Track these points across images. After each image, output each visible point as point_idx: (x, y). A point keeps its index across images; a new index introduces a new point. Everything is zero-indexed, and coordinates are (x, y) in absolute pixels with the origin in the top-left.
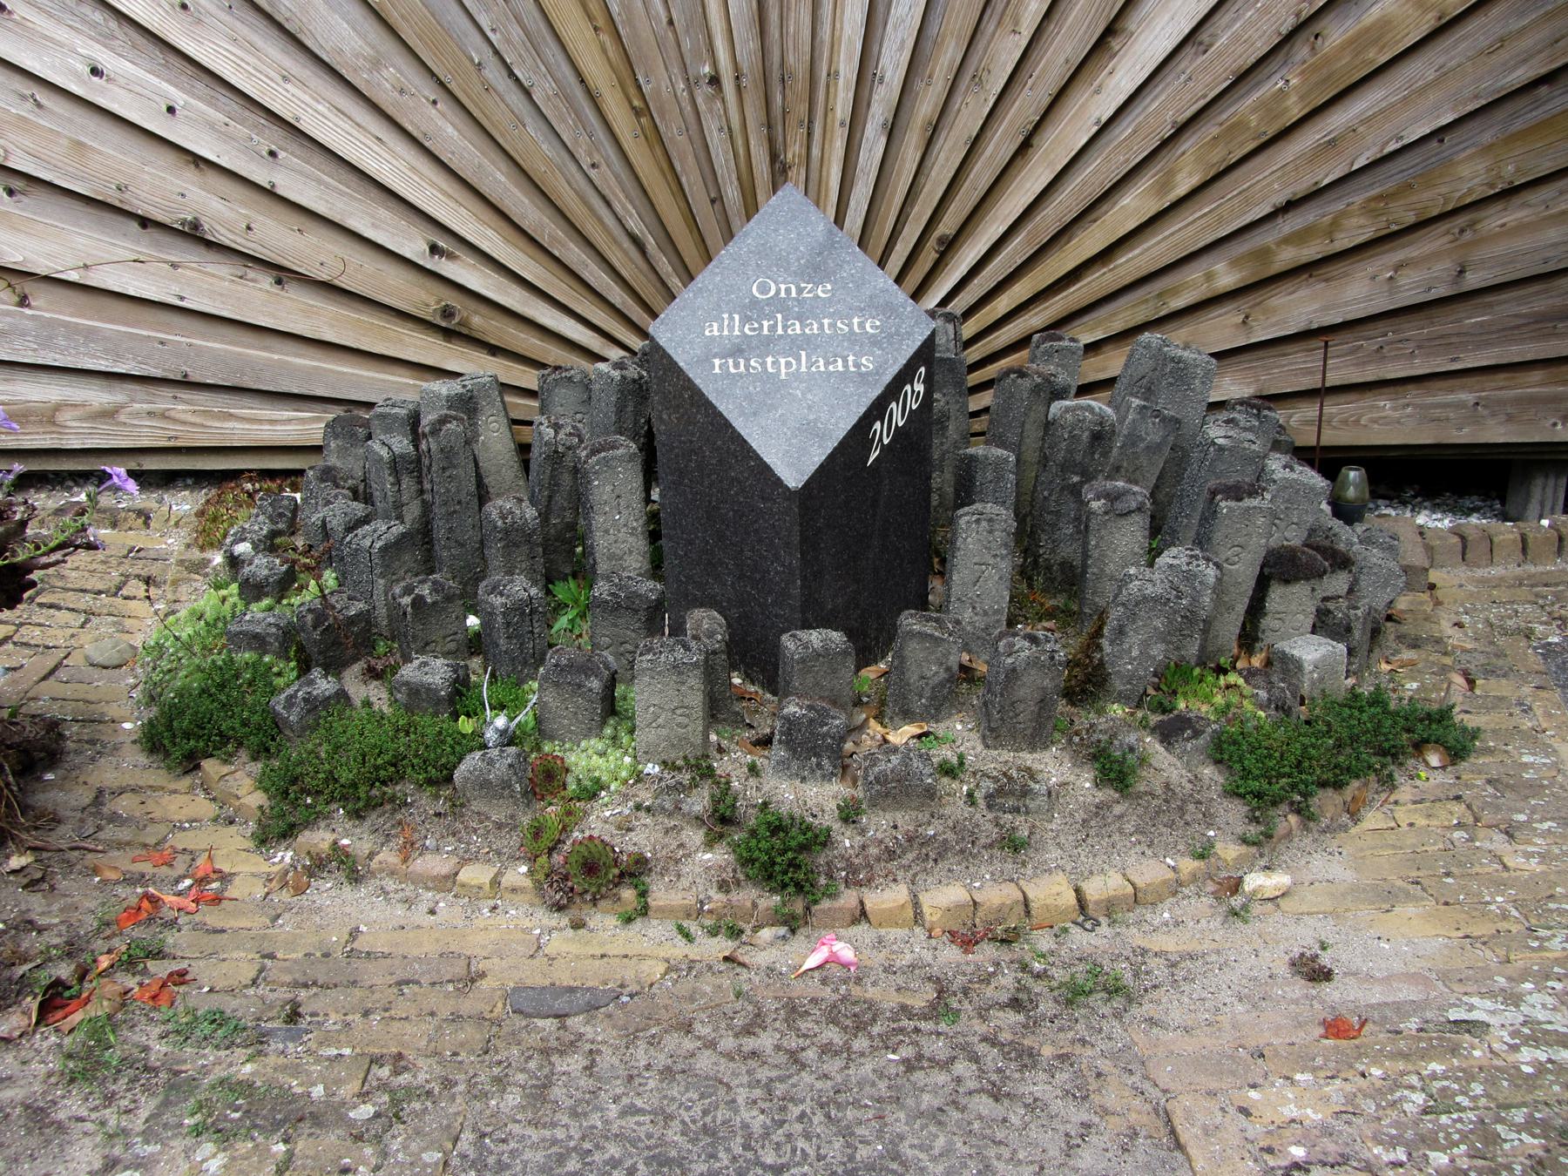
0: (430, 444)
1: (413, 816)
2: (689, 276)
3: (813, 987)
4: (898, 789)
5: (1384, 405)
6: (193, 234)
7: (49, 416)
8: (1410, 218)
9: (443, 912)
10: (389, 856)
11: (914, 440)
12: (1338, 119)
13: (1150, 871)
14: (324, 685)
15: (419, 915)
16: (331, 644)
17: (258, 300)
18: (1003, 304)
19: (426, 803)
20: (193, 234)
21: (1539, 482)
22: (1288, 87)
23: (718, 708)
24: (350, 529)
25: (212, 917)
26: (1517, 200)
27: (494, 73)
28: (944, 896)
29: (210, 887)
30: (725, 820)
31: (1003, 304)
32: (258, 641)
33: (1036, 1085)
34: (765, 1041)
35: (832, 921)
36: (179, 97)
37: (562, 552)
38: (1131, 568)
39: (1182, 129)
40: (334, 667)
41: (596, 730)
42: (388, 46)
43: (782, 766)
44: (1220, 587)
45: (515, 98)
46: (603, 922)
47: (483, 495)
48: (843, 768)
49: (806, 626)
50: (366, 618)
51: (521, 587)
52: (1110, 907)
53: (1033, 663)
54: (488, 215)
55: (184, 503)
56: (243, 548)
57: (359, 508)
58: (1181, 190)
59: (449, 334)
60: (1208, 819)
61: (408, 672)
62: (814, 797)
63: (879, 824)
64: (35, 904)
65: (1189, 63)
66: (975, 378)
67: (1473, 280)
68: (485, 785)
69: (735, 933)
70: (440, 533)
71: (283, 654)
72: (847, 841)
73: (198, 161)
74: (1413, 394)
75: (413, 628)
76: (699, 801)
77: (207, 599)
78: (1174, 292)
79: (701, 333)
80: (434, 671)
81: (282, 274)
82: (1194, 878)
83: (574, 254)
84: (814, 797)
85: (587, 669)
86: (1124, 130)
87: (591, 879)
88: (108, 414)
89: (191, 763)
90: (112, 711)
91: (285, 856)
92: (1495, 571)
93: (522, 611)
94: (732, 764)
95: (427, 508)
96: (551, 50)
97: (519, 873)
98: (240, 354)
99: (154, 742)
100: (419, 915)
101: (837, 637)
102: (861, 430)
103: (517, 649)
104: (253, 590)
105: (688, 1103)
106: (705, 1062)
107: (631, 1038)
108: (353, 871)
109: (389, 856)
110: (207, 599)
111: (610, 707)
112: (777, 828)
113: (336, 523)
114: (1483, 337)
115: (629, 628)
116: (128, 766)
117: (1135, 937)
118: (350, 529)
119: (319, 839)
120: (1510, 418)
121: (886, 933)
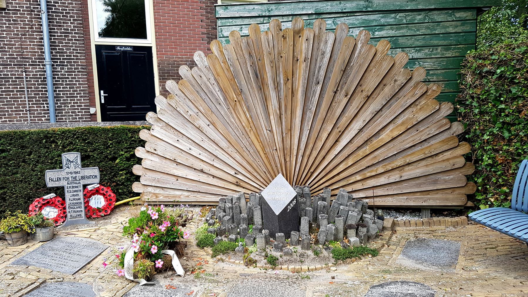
0: (234, 206)
1: (230, 255)
2: (273, 179)
3: (274, 275)
4: (286, 254)
5: (390, 199)
6: (202, 171)
7: (179, 197)
8: (391, 168)
9: (233, 265)
10: (227, 259)
11: (294, 209)
12: (376, 153)
13: (318, 266)
14: (220, 238)
15: (231, 266)
16: (220, 233)
17: (210, 180)
18: (321, 182)
19: (232, 253)
20: (202, 171)
21: (425, 211)
22: (367, 149)
23: (267, 242)
24: (223, 217)
25: (207, 265)
26: (411, 165)
27: (244, 149)
28: (291, 267)
29: (207, 262)
30: (267, 256)
31: (321, 182)
32: (211, 232)
33: (295, 285)
34: (267, 280)
35: (278, 269)
36: (201, 152)
37: (250, 221)
38: (325, 226)
39: (349, 156)
40: (221, 236)
41: (252, 245)
42: (230, 145)
43: (274, 250)
44: (336, 229)
45: (247, 152)
46: (251, 268)
47: (241, 213)
48: (282, 250)
49: (280, 232)
50: (225, 229)
51: (244, 226)
52: (312, 270)
53: (306, 239)
54: (243, 168)
55: (197, 210)
56: (208, 218)
57: (224, 214)
58: (350, 165)
59: (237, 185)
60: (329, 260)
61: (230, 237)
62: (277, 254)
63: (285, 258)
64: (188, 263)
65: (350, 146)
66: (312, 195)
67: (403, 179)
68: (239, 251)
69: (266, 270)
70: (235, 218)
71: (214, 234)
72: (280, 259)
73: (203, 161)
74: (395, 197)
75: (230, 231)
76: (264, 254)
77: (203, 226)
78: (350, 180)
79: (267, 194)
80: (233, 236)
81: (214, 177)
82: (324, 267)
83: (256, 174)
84: (277, 254)
85: (251, 237)
86: (340, 156)
87: (251, 262)
88: (188, 196)
89: (203, 248)
90: (192, 241)
91: (215, 259)
92: (411, 228)
93: (245, 229)
94: (268, 250)
95: (233, 214)
96: (253, 146)
97: (242, 262)
98: (135, 48)
99: (198, 245)
100: (231, 266)
101: (283, 234)
102: (287, 207)
103: (243, 234)
104: (210, 225)
105: (257, 284)
106: (260, 281)
107: (252, 278)
108: (223, 261)
109: (227, 259)
110: (203, 226)
111: (254, 242)
112: (272, 257)
113: (221, 216)
114: (406, 188)
115: (257, 232)
116: (195, 248)
117: (314, 273)
118: (223, 217)
119: (219, 257)
120: (414, 201)
121: (285, 270)
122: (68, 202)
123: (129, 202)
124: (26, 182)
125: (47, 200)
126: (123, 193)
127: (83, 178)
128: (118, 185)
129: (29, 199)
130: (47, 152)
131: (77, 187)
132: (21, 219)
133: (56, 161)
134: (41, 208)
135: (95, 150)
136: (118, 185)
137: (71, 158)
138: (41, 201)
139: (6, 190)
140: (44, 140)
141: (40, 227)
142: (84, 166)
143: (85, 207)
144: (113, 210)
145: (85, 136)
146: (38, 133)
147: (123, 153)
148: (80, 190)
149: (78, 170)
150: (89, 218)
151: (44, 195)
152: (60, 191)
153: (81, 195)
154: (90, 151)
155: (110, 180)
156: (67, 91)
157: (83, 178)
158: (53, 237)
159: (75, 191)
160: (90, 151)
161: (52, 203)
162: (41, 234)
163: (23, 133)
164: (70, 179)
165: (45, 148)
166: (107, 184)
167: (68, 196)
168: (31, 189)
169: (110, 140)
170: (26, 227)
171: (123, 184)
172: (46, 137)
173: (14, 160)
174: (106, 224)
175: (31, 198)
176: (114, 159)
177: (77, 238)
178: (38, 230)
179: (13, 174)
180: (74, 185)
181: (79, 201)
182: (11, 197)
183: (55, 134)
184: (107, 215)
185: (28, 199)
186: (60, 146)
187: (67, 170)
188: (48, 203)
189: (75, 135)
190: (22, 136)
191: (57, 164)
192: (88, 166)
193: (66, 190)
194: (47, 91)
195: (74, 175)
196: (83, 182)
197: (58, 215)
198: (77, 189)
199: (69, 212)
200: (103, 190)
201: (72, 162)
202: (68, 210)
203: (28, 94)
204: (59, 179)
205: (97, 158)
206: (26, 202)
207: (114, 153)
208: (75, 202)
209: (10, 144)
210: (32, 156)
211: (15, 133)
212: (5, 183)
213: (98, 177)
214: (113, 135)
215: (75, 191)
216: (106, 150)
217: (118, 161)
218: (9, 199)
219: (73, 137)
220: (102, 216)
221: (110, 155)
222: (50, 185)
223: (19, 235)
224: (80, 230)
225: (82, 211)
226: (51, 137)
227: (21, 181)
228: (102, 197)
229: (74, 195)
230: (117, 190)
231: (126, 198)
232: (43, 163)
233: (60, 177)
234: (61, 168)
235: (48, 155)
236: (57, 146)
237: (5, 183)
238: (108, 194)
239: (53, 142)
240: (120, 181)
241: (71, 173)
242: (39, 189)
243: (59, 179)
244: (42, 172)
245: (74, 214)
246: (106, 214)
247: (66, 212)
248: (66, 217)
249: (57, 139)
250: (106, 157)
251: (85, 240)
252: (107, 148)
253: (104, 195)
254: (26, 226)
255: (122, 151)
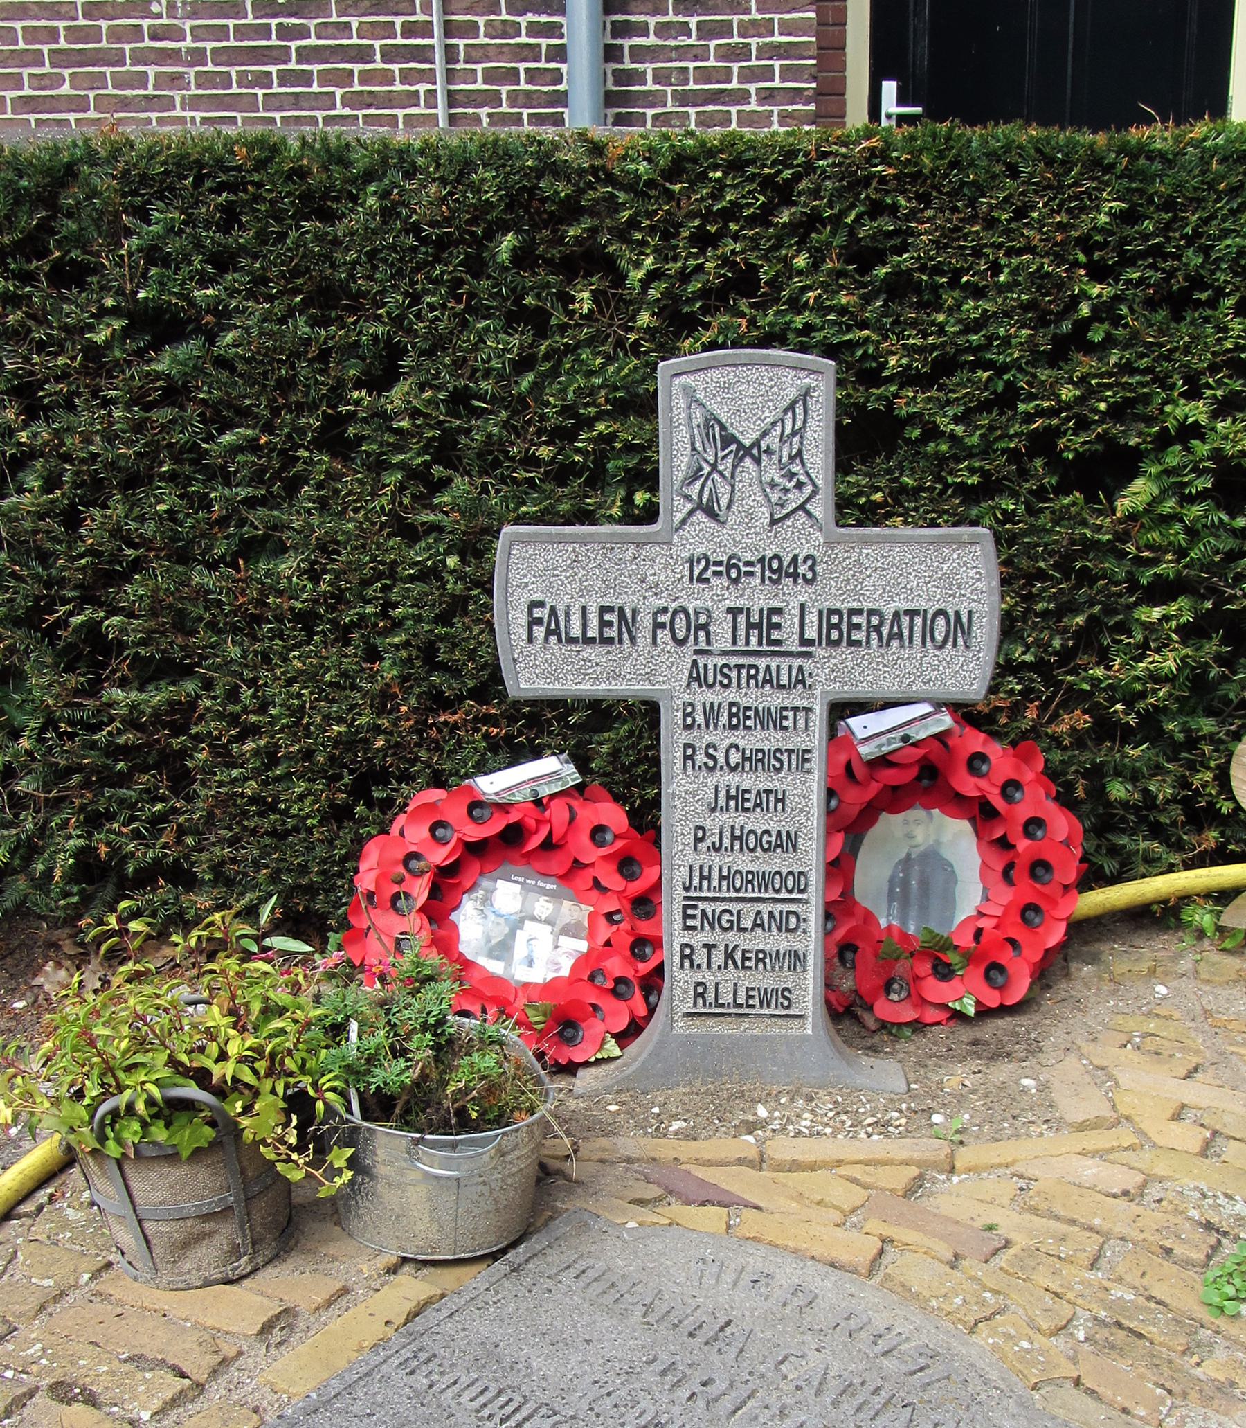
122: (679, 858)
123: (1186, 899)
124: (343, 634)
125: (503, 808)
126: (1145, 815)
127: (839, 629)
128: (1106, 729)
129: (366, 788)
130: (524, 363)
131: (773, 720)
132: (216, 1003)
133: (600, 458)
134: (439, 909)
135: (945, 366)
136: (1106, 729)
137: (743, 406)
138: (456, 813)
139: (190, 686)
140: (509, 241)
141: (405, 1123)
142: (854, 510)
143: (831, 912)
144: (1049, 971)
145: (876, 209)
146: (459, 169)
147: (1197, 412)
148: (804, 756)
149: (799, 541)
150: (844, 1012)
151: (483, 768)
152: (618, 745)
153: (807, 793)
154: (907, 378)
155: (1050, 681)
156: (682, 52)
157: (839, 629)
158: (542, 1201)
159: (755, 760)
160: (907, 378)
161: (549, 845)
162: (418, 1183)
163: (337, 156)
164: (722, 639)
165: (516, 317)
166: (1016, 711)
167: (684, 796)
168: (383, 702)
169: (1098, 273)
170: (264, 1122)
171: (1150, 727)
172: (522, 204)
173: (244, 414)
174: (1008, 1113)
175: (382, 777)
176: (1107, 470)
177: (755, 1260)
178: (388, 1143)
179: (251, 549)
180: (752, 697)
181: (779, 862)
182: (223, 756)
183: (611, 179)
184: (1004, 1010)
185: (360, 790)
186: (638, 304)
187: (700, 537)
188: (510, 842)
189: (783, 193)
190: (318, 185)
191: (607, 476)
192: (870, 515)
193: (673, 740)
194: (559, 54)
195: (757, 596)
196: (834, 673)
197: (588, 968)
198: (770, 740)
199: (687, 956)
200: (976, 761)
201: (753, 452)
202: (675, 936)
203: (450, 75)
204: (615, 626)
205: (961, 451)
206: (338, 814)
207: (1117, 412)
208: (744, 862)
209: (223, 261)
210: (397, 395)
211: (267, 152)
212: (183, 624)
213: (986, 631)
214: (1129, 217)
215: (755, 760)
216: (1044, 374)
217: (1138, 492)
218: (208, 771)
219: (763, 218)
220: (958, 1016)
221: (1083, 425)
222: (534, 672)
223: (195, 1187)
224: (783, 1148)
225: (797, 959)
226: (571, 210)
227: (307, 620)
228: (965, 826)
229: (738, 798)
230: (1096, 775)
231: (1154, 866)
232: (491, 459)
233: (629, 601)
234: (650, 514)
235: (536, 387)
236: (614, 300)
237: (183, 624)
238: (1024, 811)
239: (592, 261)
240: (1130, 700)
241: (733, 570)
242: (439, 701)
243: (615, 626)
244: (476, 546)
245: (728, 983)
246: (993, 1000)
247: (657, 943)
248: (653, 982)
249: (622, 233)
250: (1044, 443)
251: (827, 1286)
252: (1058, 355)
253: (982, 814)
254: (269, 1105)
255: (1193, 393)
